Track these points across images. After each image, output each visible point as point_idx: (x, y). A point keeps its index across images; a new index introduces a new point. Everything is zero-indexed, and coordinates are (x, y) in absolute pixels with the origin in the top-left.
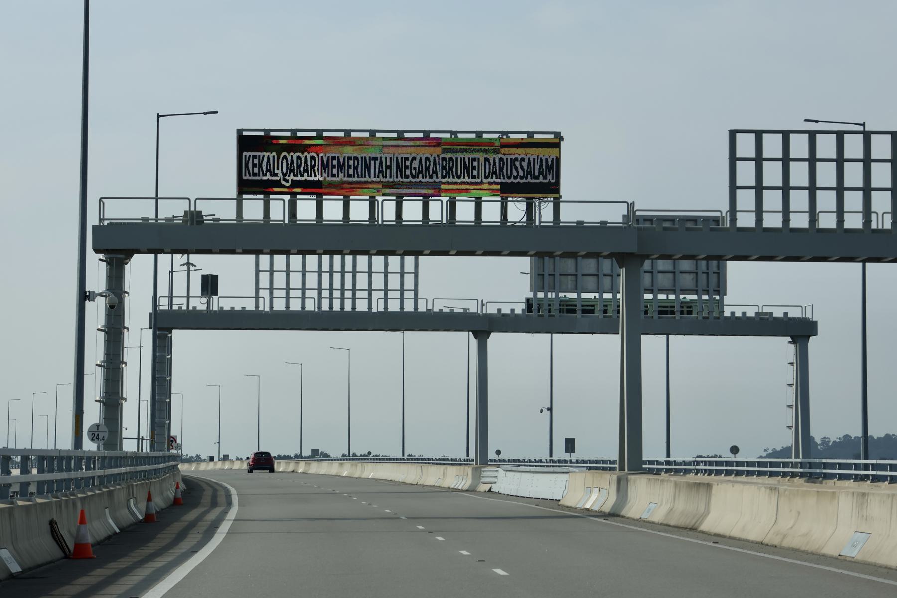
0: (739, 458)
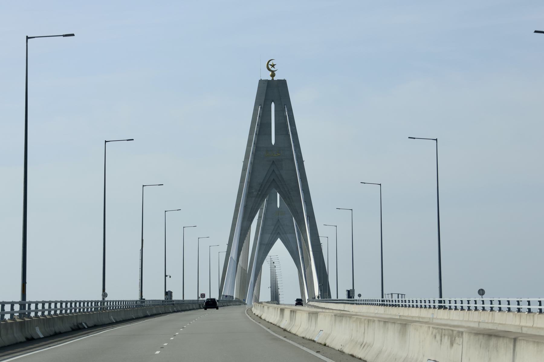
0: (361, 298)
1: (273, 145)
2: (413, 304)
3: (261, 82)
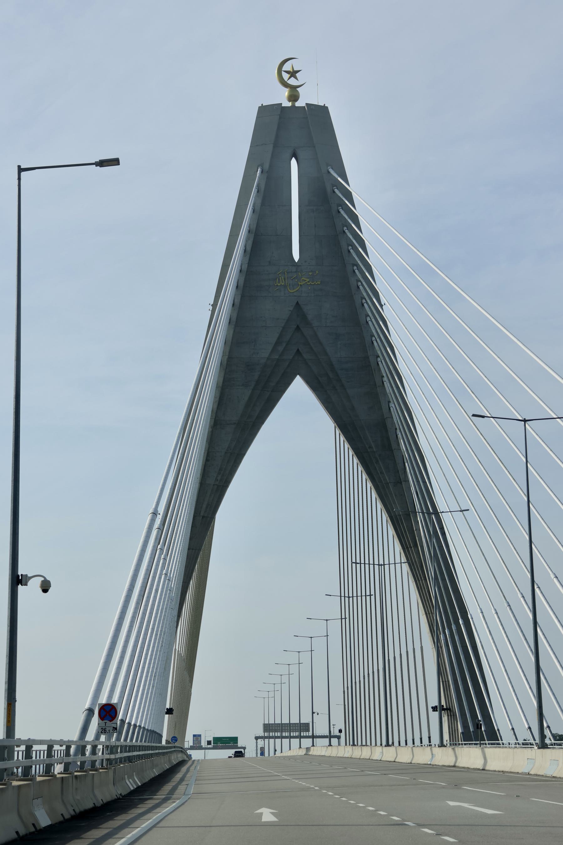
1: (296, 262)
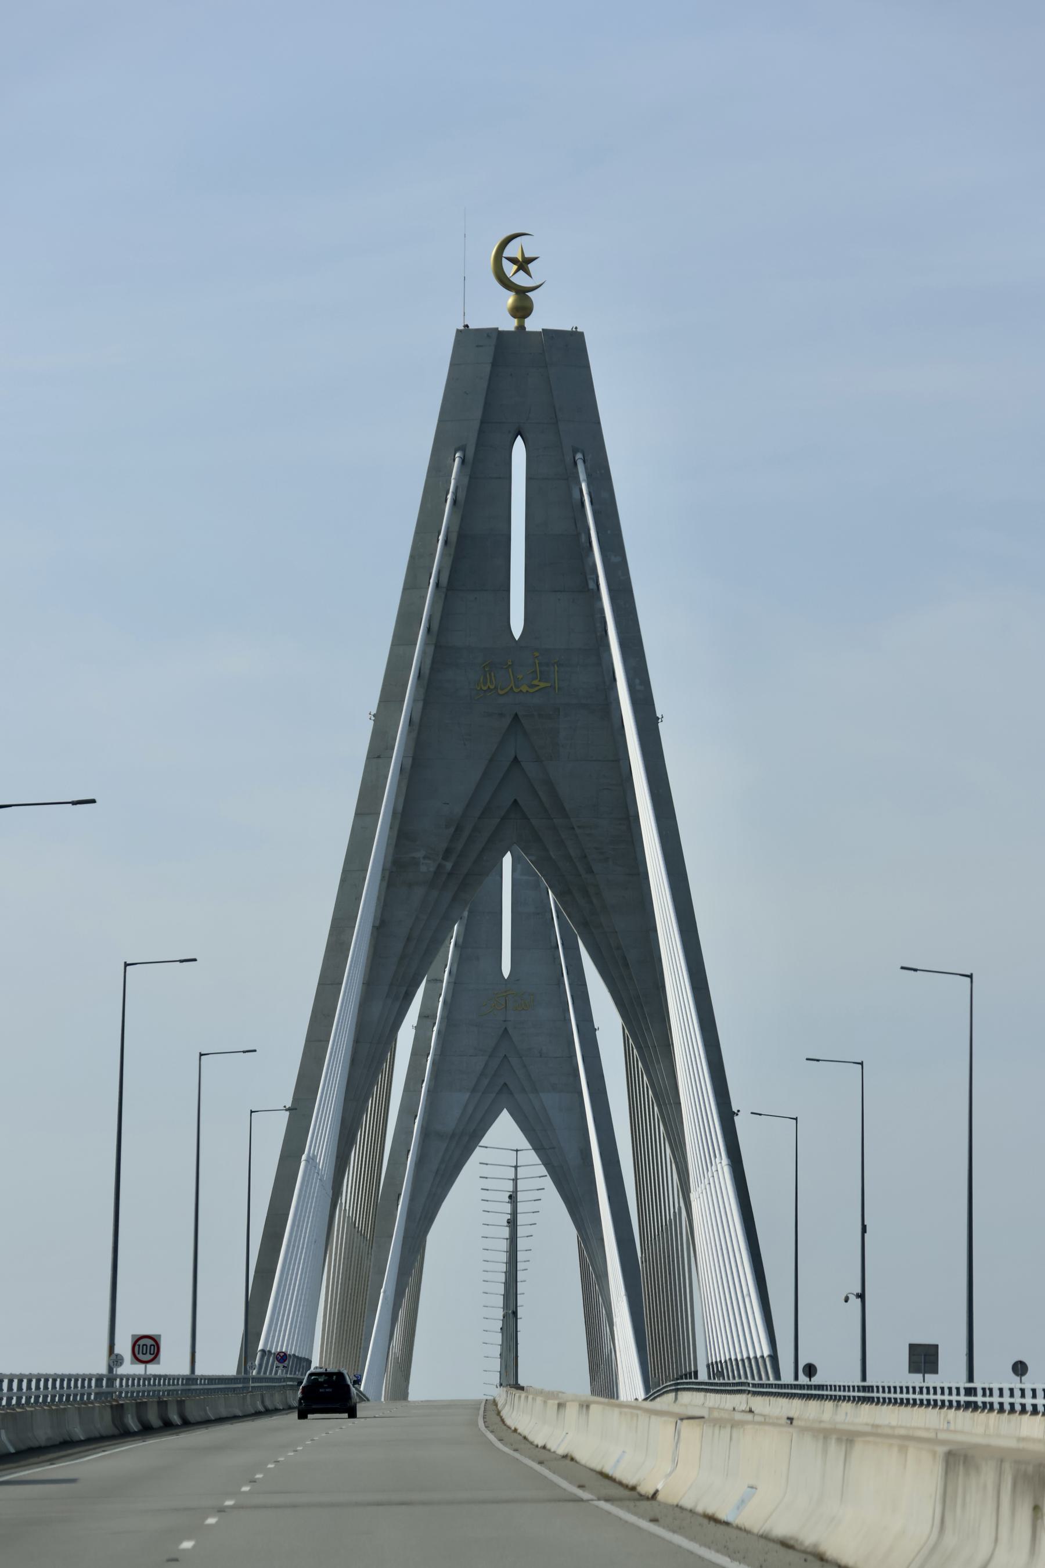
1: (517, 638)
2: (1034, 1401)
3: (466, 337)
